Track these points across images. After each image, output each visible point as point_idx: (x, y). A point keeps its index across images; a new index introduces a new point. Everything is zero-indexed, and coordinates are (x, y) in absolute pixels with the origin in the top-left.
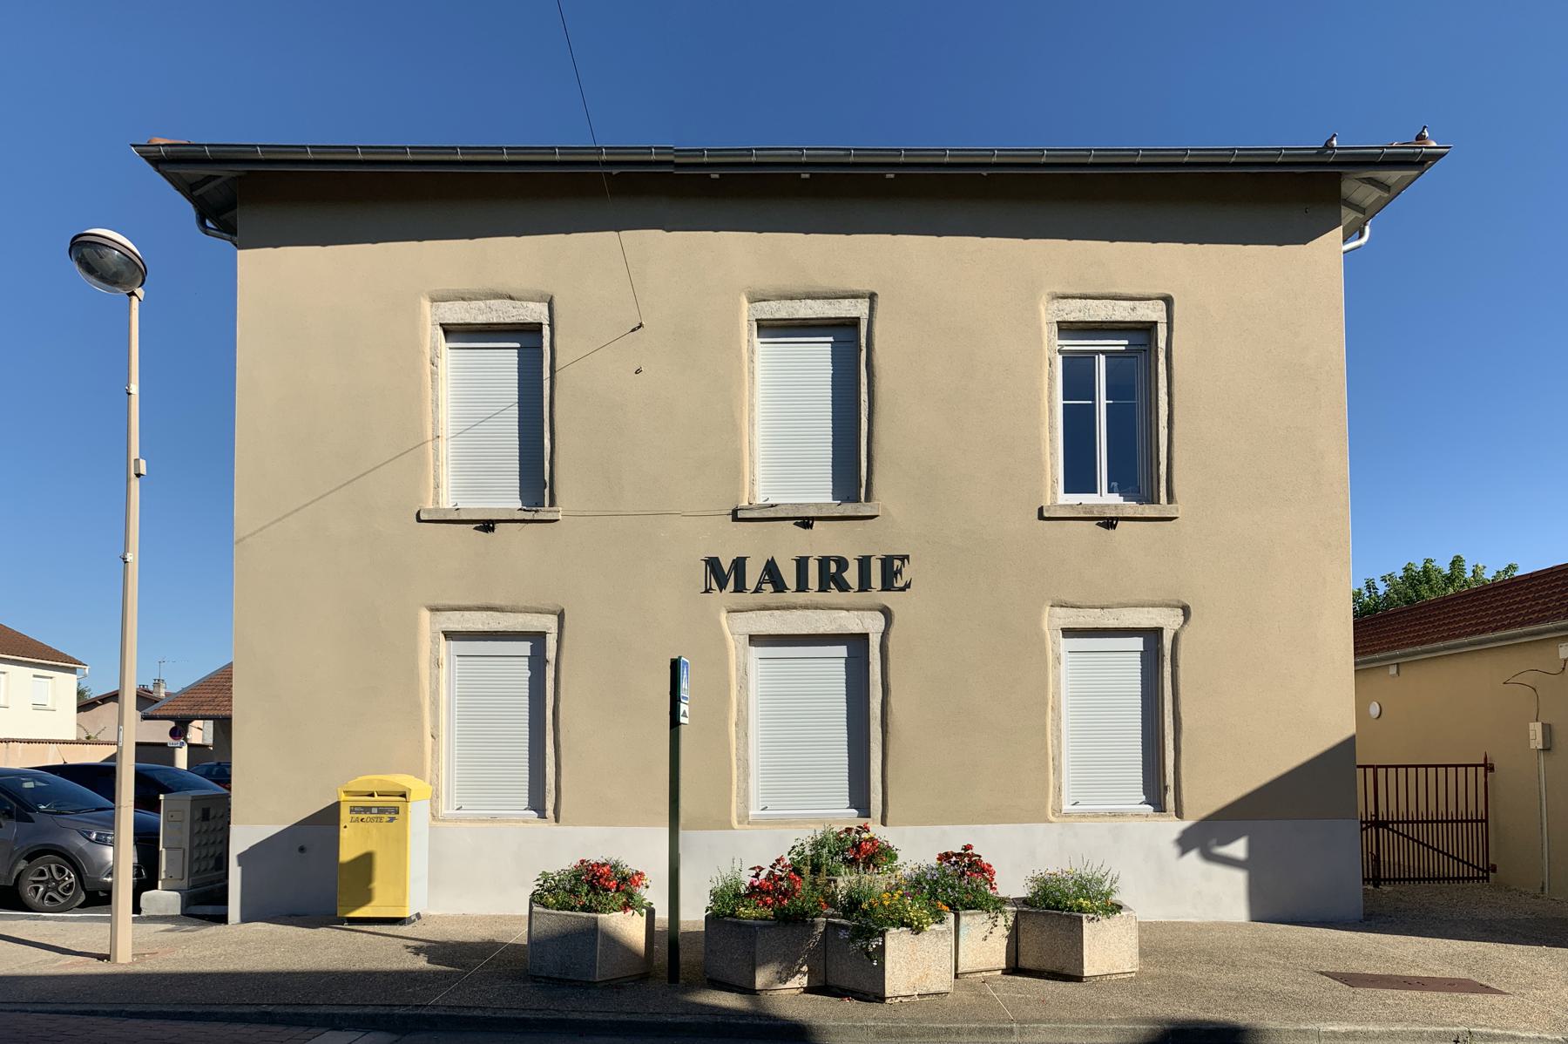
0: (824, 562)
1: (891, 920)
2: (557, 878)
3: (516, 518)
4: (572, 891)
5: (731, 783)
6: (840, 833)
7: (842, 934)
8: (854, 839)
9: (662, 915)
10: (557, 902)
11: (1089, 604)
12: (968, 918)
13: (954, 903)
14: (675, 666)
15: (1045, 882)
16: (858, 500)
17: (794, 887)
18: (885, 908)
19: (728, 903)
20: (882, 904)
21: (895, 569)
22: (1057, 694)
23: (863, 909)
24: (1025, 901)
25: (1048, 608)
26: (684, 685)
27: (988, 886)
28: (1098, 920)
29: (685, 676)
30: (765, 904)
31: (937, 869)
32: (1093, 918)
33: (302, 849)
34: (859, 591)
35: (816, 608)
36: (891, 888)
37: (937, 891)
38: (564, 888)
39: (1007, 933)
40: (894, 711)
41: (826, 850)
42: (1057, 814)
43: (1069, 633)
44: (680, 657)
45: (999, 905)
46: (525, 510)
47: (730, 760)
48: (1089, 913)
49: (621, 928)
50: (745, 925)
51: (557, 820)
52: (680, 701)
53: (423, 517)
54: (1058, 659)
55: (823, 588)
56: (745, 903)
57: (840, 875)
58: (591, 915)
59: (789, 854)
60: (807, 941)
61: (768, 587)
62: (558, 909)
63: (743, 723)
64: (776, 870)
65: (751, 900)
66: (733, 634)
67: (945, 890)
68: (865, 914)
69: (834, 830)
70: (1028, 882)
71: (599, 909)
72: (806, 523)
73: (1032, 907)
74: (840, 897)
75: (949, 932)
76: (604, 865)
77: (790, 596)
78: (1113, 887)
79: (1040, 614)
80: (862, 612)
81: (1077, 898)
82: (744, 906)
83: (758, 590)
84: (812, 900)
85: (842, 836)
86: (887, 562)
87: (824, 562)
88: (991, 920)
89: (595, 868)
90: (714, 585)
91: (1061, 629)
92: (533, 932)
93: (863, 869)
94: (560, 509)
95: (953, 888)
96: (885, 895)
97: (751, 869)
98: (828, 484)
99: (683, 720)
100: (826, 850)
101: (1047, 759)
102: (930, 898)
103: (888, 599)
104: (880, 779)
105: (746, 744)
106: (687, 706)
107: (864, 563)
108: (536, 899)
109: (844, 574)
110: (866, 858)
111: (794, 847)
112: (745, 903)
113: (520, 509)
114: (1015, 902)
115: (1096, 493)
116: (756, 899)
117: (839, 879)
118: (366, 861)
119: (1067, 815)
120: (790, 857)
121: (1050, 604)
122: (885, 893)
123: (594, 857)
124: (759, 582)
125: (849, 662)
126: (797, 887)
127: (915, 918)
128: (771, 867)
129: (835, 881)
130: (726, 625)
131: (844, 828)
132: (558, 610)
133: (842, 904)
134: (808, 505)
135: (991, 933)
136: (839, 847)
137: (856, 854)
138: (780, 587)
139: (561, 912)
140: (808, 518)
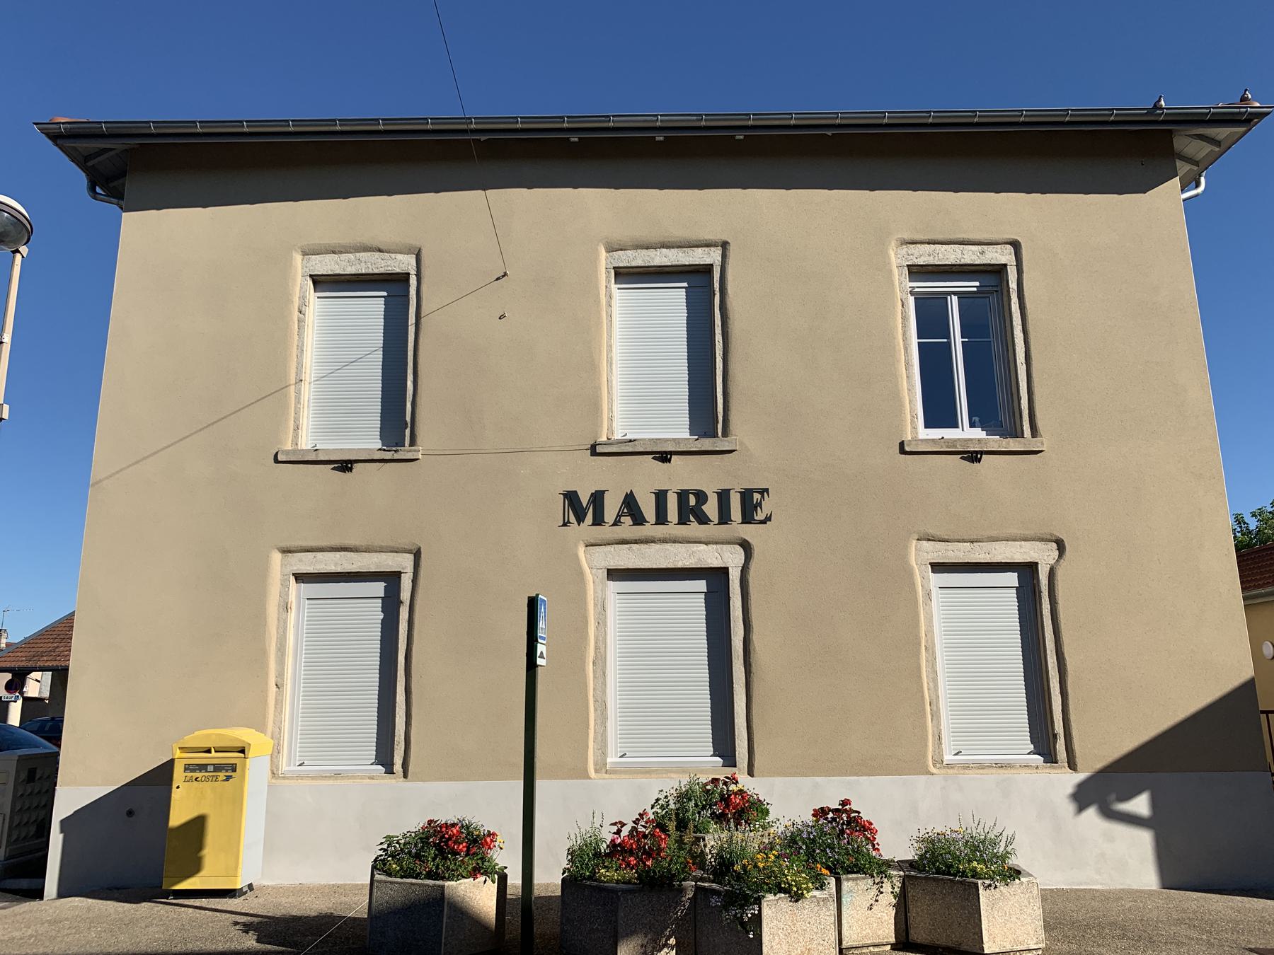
0: (683, 495)
1: (767, 884)
2: (402, 841)
3: (375, 458)
4: (418, 856)
6: (707, 784)
9: (515, 879)
12: (850, 883)
14: (533, 604)
15: (932, 842)
16: (715, 435)
19: (587, 864)
20: (756, 866)
22: (930, 632)
24: (911, 864)
25: (914, 542)
26: (541, 624)
27: (870, 847)
28: (996, 887)
29: (543, 614)
30: (628, 865)
32: (990, 885)
33: (130, 813)
34: (719, 524)
35: (675, 542)
36: (765, 848)
37: (814, 851)
39: (894, 901)
43: (938, 567)
44: (537, 595)
45: (884, 868)
46: (384, 450)
48: (985, 878)
51: (405, 776)
52: (537, 641)
53: (280, 459)
55: (683, 521)
57: (708, 832)
60: (675, 908)
61: (627, 520)
62: (402, 877)
63: (600, 660)
64: (639, 826)
65: (612, 860)
70: (914, 842)
71: (447, 875)
72: (664, 457)
73: (921, 872)
74: (710, 856)
76: (454, 825)
77: (649, 529)
78: (1009, 849)
81: (970, 861)
82: (605, 867)
83: (617, 523)
84: (680, 860)
85: (708, 787)
86: (746, 495)
87: (683, 495)
90: (572, 519)
91: (930, 564)
95: (832, 849)
96: (759, 856)
97: (612, 824)
99: (540, 661)
102: (808, 859)
103: (748, 532)
105: (604, 684)
107: (723, 496)
110: (735, 813)
111: (658, 800)
113: (380, 449)
114: (901, 865)
115: (958, 427)
116: (618, 859)
118: (198, 825)
119: (950, 766)
120: (654, 810)
123: (444, 817)
124: (618, 515)
125: (709, 596)
126: (663, 845)
127: (793, 883)
128: (634, 822)
129: (704, 840)
130: (584, 559)
131: (710, 779)
132: (414, 548)
134: (666, 440)
135: (877, 901)
136: (706, 800)
137: (724, 808)
138: (639, 519)
140: (666, 452)
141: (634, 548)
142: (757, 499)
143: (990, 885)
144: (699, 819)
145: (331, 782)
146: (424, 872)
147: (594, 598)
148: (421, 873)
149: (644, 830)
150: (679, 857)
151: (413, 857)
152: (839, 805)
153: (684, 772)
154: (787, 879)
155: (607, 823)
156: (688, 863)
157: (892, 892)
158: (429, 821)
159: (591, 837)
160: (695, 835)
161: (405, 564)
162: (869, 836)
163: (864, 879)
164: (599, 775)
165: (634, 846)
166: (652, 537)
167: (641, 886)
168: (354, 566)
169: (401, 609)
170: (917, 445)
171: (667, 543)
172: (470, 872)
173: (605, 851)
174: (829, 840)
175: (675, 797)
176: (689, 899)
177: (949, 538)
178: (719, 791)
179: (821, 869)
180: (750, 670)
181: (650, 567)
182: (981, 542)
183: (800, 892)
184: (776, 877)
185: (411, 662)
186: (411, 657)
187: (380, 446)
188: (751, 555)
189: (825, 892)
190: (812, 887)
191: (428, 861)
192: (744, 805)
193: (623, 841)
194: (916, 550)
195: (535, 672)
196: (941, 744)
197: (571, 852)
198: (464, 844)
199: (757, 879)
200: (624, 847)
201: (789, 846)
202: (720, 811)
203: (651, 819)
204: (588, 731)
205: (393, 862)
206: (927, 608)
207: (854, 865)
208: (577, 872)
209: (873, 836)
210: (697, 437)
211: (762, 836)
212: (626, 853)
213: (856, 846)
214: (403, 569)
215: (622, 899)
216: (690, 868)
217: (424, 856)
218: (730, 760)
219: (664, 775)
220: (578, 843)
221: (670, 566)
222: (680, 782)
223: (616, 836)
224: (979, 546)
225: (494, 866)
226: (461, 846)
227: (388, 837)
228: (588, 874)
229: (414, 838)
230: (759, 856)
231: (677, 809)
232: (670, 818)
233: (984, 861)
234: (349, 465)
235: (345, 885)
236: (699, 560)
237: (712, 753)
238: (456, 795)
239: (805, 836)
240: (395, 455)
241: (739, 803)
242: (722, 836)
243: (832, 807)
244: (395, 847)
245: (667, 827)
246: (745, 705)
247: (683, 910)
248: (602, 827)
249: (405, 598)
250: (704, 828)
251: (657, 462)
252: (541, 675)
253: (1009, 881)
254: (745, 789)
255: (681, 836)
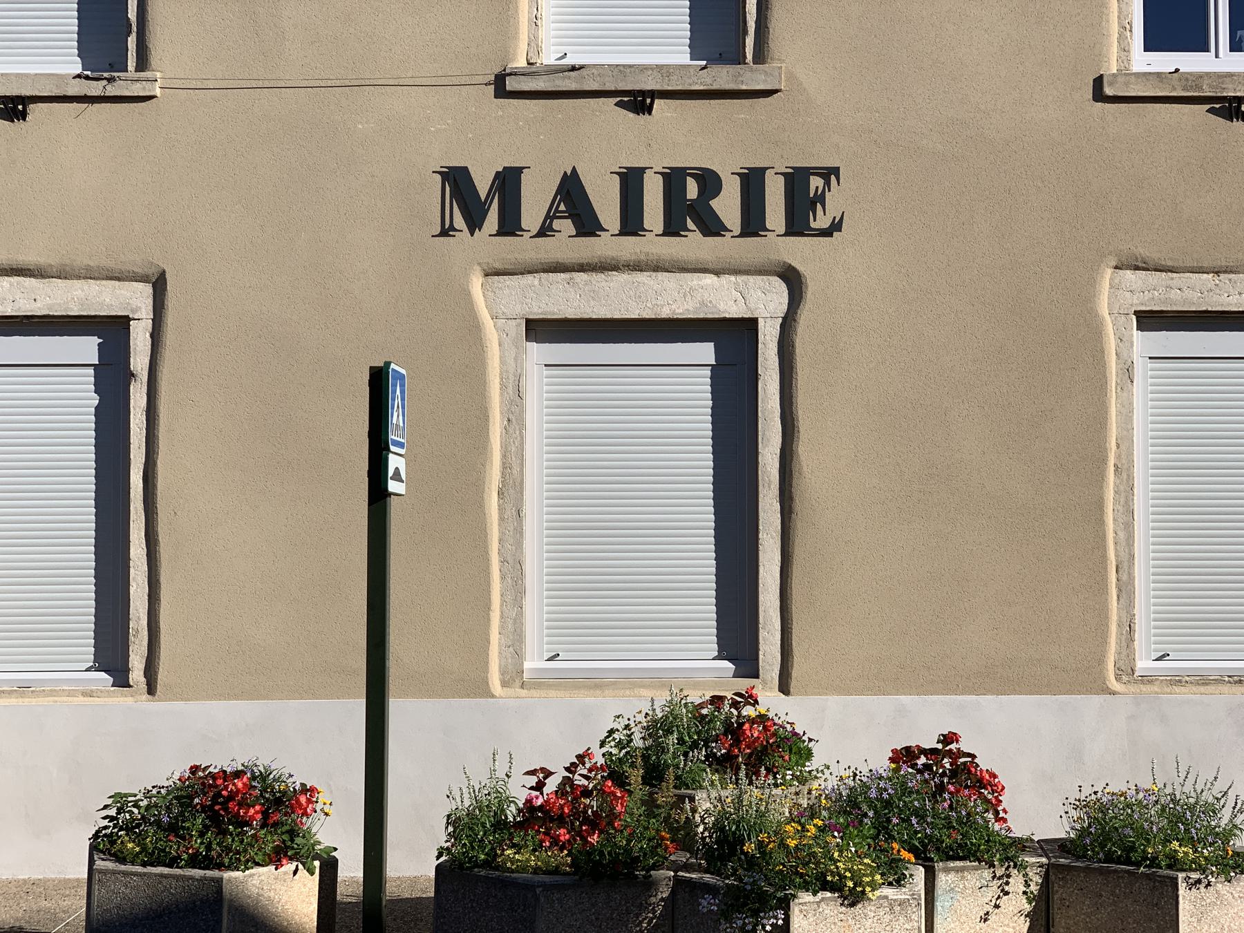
0: (673, 179)
1: (801, 876)
2: (144, 803)
3: (70, 93)
4: (173, 828)
5: (488, 607)
6: (701, 706)
7: (705, 903)
8: (728, 718)
9: (351, 870)
10: (144, 849)
11: (1189, 263)
12: (952, 877)
13: (925, 846)
14: (379, 380)
15: (1103, 809)
16: (739, 59)
17: (612, 809)
18: (789, 853)
19: (481, 841)
20: (783, 845)
21: (812, 195)
22: (1126, 440)
23: (746, 854)
24: (1062, 846)
25: (1109, 271)
26: (396, 418)
27: (990, 816)
28: (1209, 884)
29: (398, 401)
30: (555, 841)
31: (890, 779)
32: (1199, 881)
34: (742, 235)
36: (801, 815)
37: (889, 821)
38: (158, 823)
39: (1028, 908)
40: (805, 469)
41: (673, 738)
42: (1125, 678)
43: (1150, 320)
44: (388, 364)
45: (1012, 852)
46: (87, 78)
47: (487, 560)
48: (1191, 870)
49: (269, 899)
50: (514, 883)
51: (151, 690)
52: (388, 450)
53: (1109, 91)
54: (1128, 372)
55: (673, 228)
56: (516, 840)
57: (701, 787)
58: (209, 873)
59: (602, 744)
60: (637, 916)
61: (565, 226)
62: (144, 865)
63: (512, 489)
64: (576, 777)
65: (526, 834)
66: (494, 317)
67: (908, 820)
68: (751, 862)
69: (689, 700)
70: (1070, 809)
71: (226, 861)
72: (639, 102)
73: (1078, 858)
74: (701, 829)
75: (914, 903)
76: (238, 774)
77: (608, 245)
78: (1238, 821)
79: (1093, 283)
80: (745, 278)
81: (1167, 841)
82: (514, 846)
83: (545, 231)
84: (648, 834)
85: (705, 711)
86: (796, 180)
87: (673, 179)
88: (996, 883)
89: (219, 782)
90: (459, 222)
91: (1136, 313)
92: (95, 910)
93: (747, 775)
94: (158, 75)
95: (922, 818)
96: (788, 828)
97: (528, 773)
98: (683, 29)
99: (393, 486)
100: (673, 738)
101: (1105, 569)
102: (878, 835)
103: (798, 251)
104: (778, 603)
105: (519, 531)
106: (402, 460)
107: (752, 181)
108: (101, 845)
109: (713, 203)
110: (750, 755)
111: (611, 732)
112: (516, 840)
113: (79, 76)
114: (1044, 847)
115: (1208, 50)
116: (538, 832)
117: (700, 795)
119: (1147, 679)
120: (604, 750)
121: (1114, 264)
122: (788, 823)
123: (219, 760)
124: (547, 216)
125: (720, 375)
126: (619, 808)
127: (848, 874)
128: (567, 769)
129: (692, 799)
130: (482, 299)
131: (708, 698)
132: (153, 272)
133: (705, 845)
134: (644, 68)
135: (997, 906)
136: (698, 733)
137: (731, 745)
138: (587, 225)
139: (150, 869)
140: (643, 93)
141: (578, 280)
142: (817, 188)
143: (1199, 881)
144: (685, 765)
145: (13, 701)
146: (185, 856)
147: (501, 374)
148: (179, 857)
149: (585, 782)
150: (646, 828)
151: (165, 830)
152: (938, 743)
153: (662, 686)
154: (837, 868)
155: (518, 772)
156: (663, 838)
157: (1025, 893)
158: (191, 768)
159: (489, 794)
160: (677, 792)
161: (135, 303)
162: (990, 797)
163: (976, 869)
164: (509, 691)
165: (566, 810)
166: (613, 259)
167: (577, 877)
168: (38, 304)
169: (132, 387)
170: (1127, 84)
171: (641, 271)
172: (269, 855)
173: (514, 819)
174: (916, 803)
175: (643, 728)
176: (662, 899)
177: (1176, 264)
178: (722, 717)
179: (899, 851)
180: (790, 506)
181: (609, 316)
182: (1231, 272)
183: (859, 889)
184: (817, 864)
185: (155, 486)
186: (154, 477)
187: (78, 69)
188: (801, 297)
189: (904, 889)
190: (881, 881)
191: (192, 836)
192: (768, 742)
193: (547, 802)
194: (1111, 286)
195: (385, 503)
196: (1133, 640)
197: (453, 820)
198: (258, 808)
199: (784, 866)
200: (549, 811)
201: (845, 812)
202: (723, 751)
203: (599, 765)
204: (488, 615)
205: (127, 838)
206: (1125, 394)
207: (960, 846)
208: (464, 853)
209: (996, 798)
210: (704, 63)
211: (797, 794)
212: (551, 822)
213: (964, 813)
214: (133, 311)
215: (542, 899)
216: (667, 847)
217: (183, 828)
218: (747, 665)
219: (628, 692)
220: (467, 803)
221: (647, 314)
222: (652, 700)
223: (535, 793)
224: (1230, 280)
225: (313, 845)
226: (252, 811)
227: (118, 797)
228: (483, 857)
229: (164, 797)
230: (788, 828)
231: (647, 749)
232: (633, 762)
233: (1192, 842)
234: (20, 107)
235: (46, 881)
236: (703, 303)
237: (716, 654)
238: (247, 725)
239: (873, 795)
240: (109, 88)
241: (758, 738)
242: (724, 793)
243: (927, 745)
244: (131, 812)
245: (627, 778)
246: (778, 569)
247: (652, 919)
248: (508, 776)
249: (139, 369)
250: (694, 781)
251: (625, 112)
252: (396, 510)
253: (1232, 874)
254: (771, 715)
255: (651, 794)
